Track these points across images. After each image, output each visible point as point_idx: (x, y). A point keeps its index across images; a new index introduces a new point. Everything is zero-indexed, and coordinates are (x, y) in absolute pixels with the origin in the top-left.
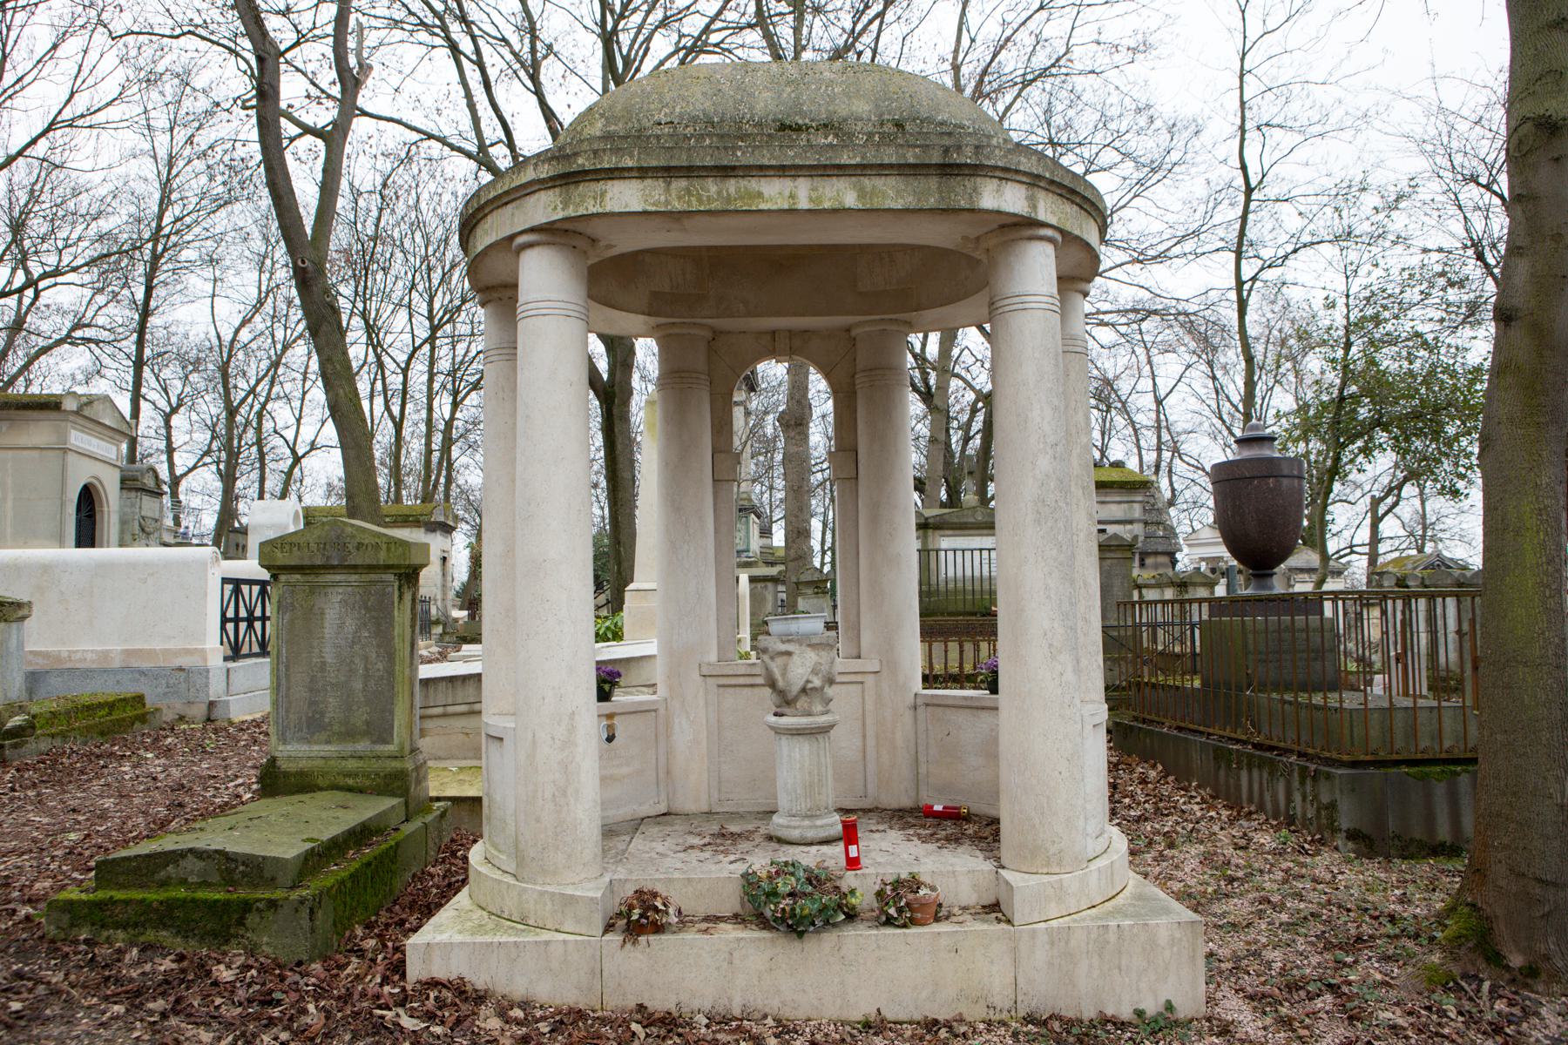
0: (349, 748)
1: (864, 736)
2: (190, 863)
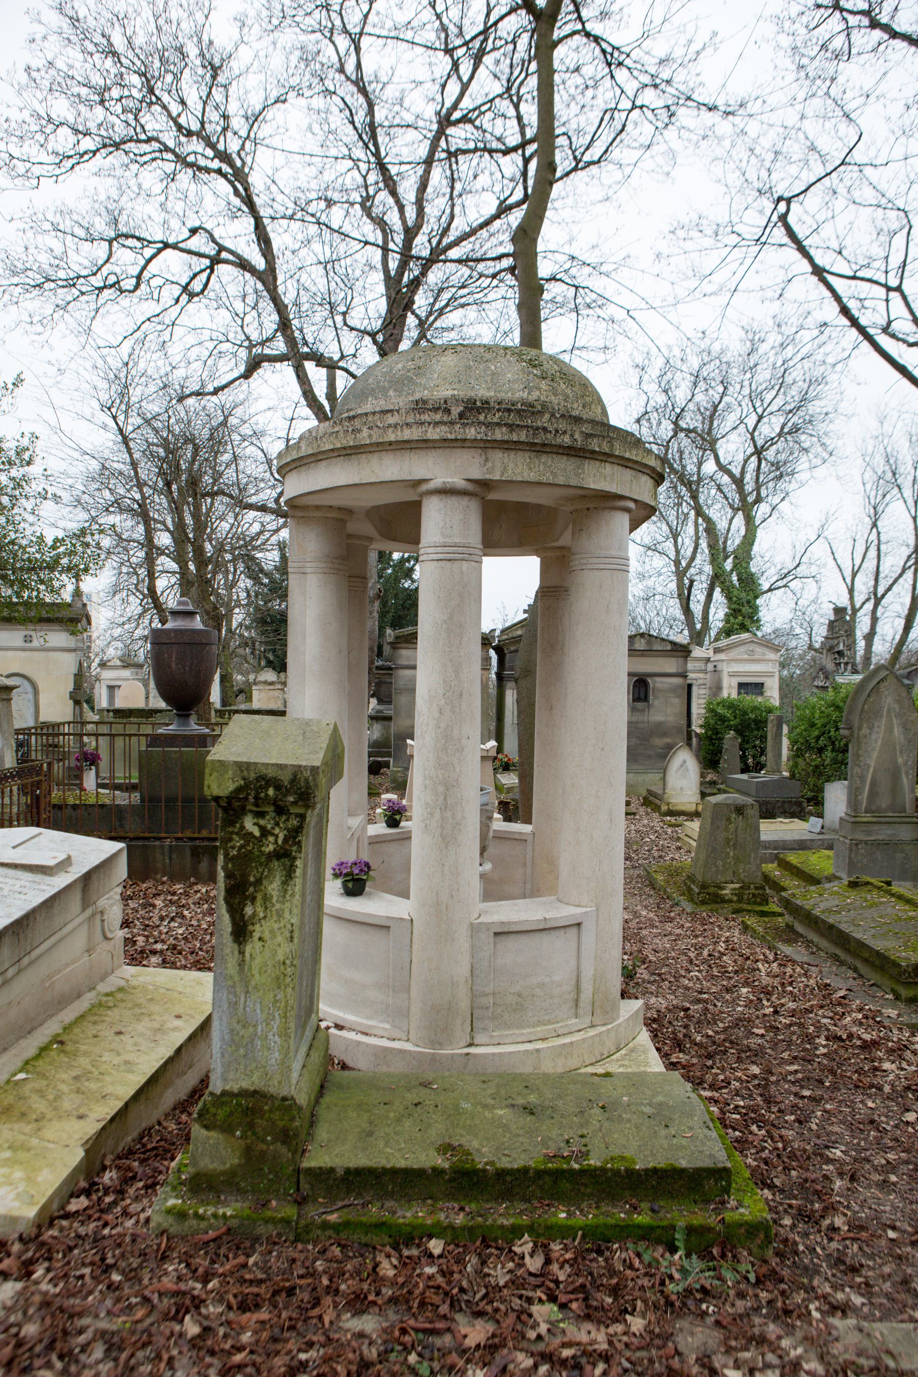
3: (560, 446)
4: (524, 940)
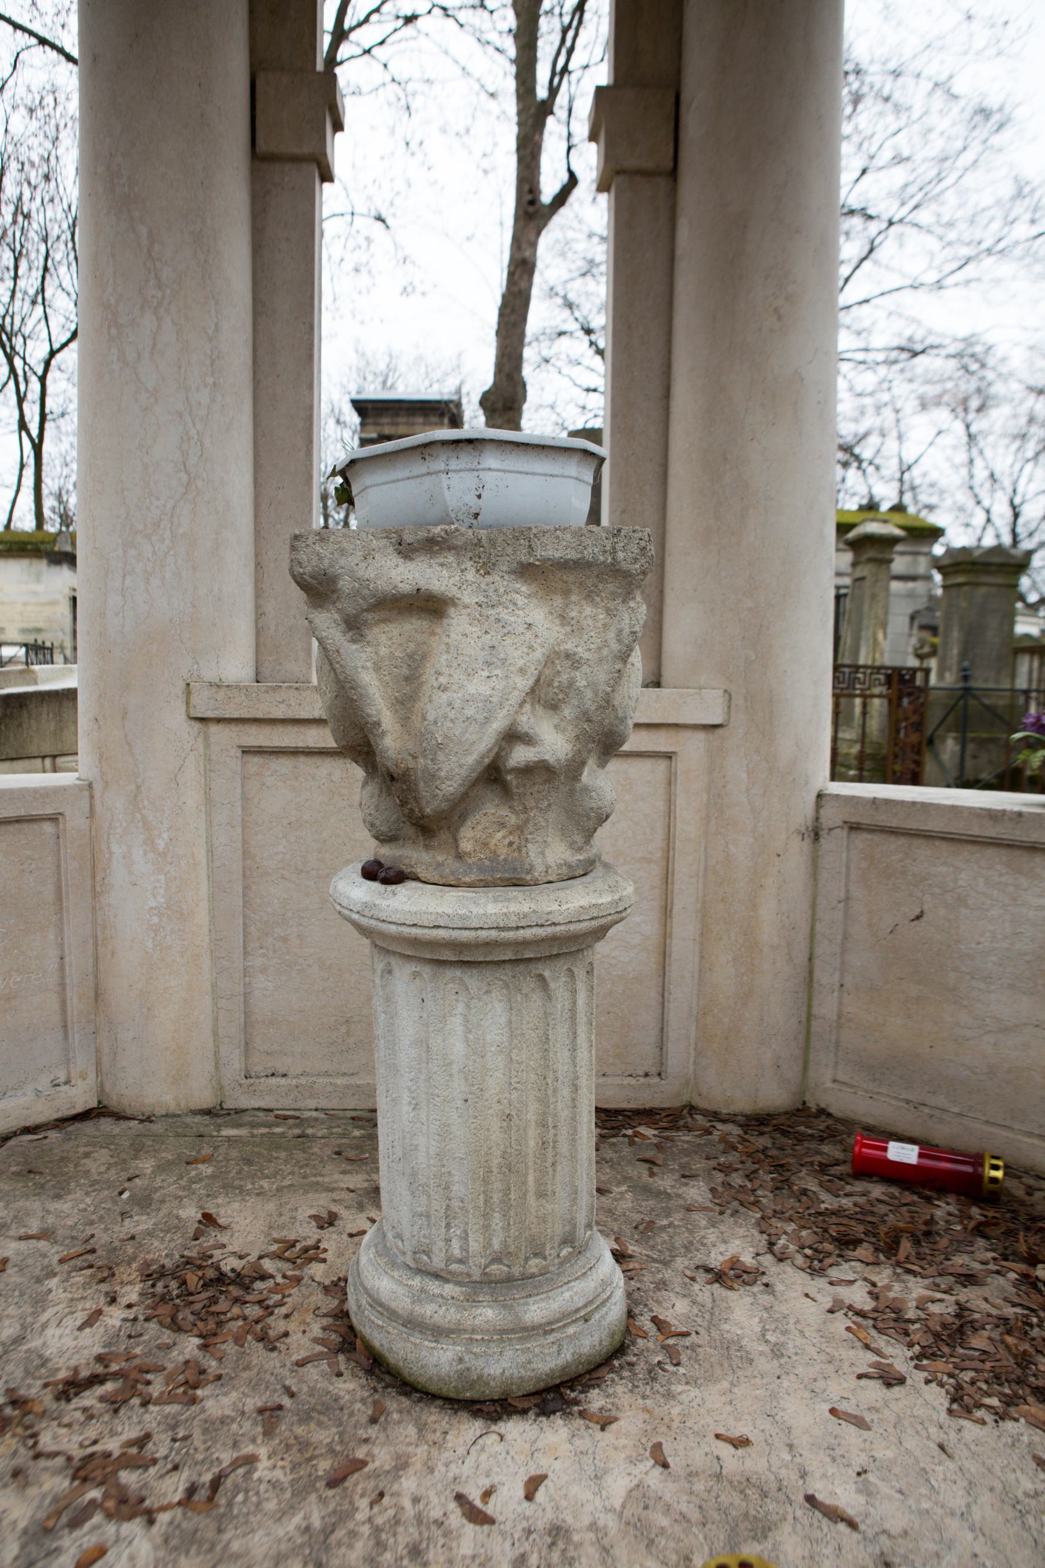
1: (666, 912)
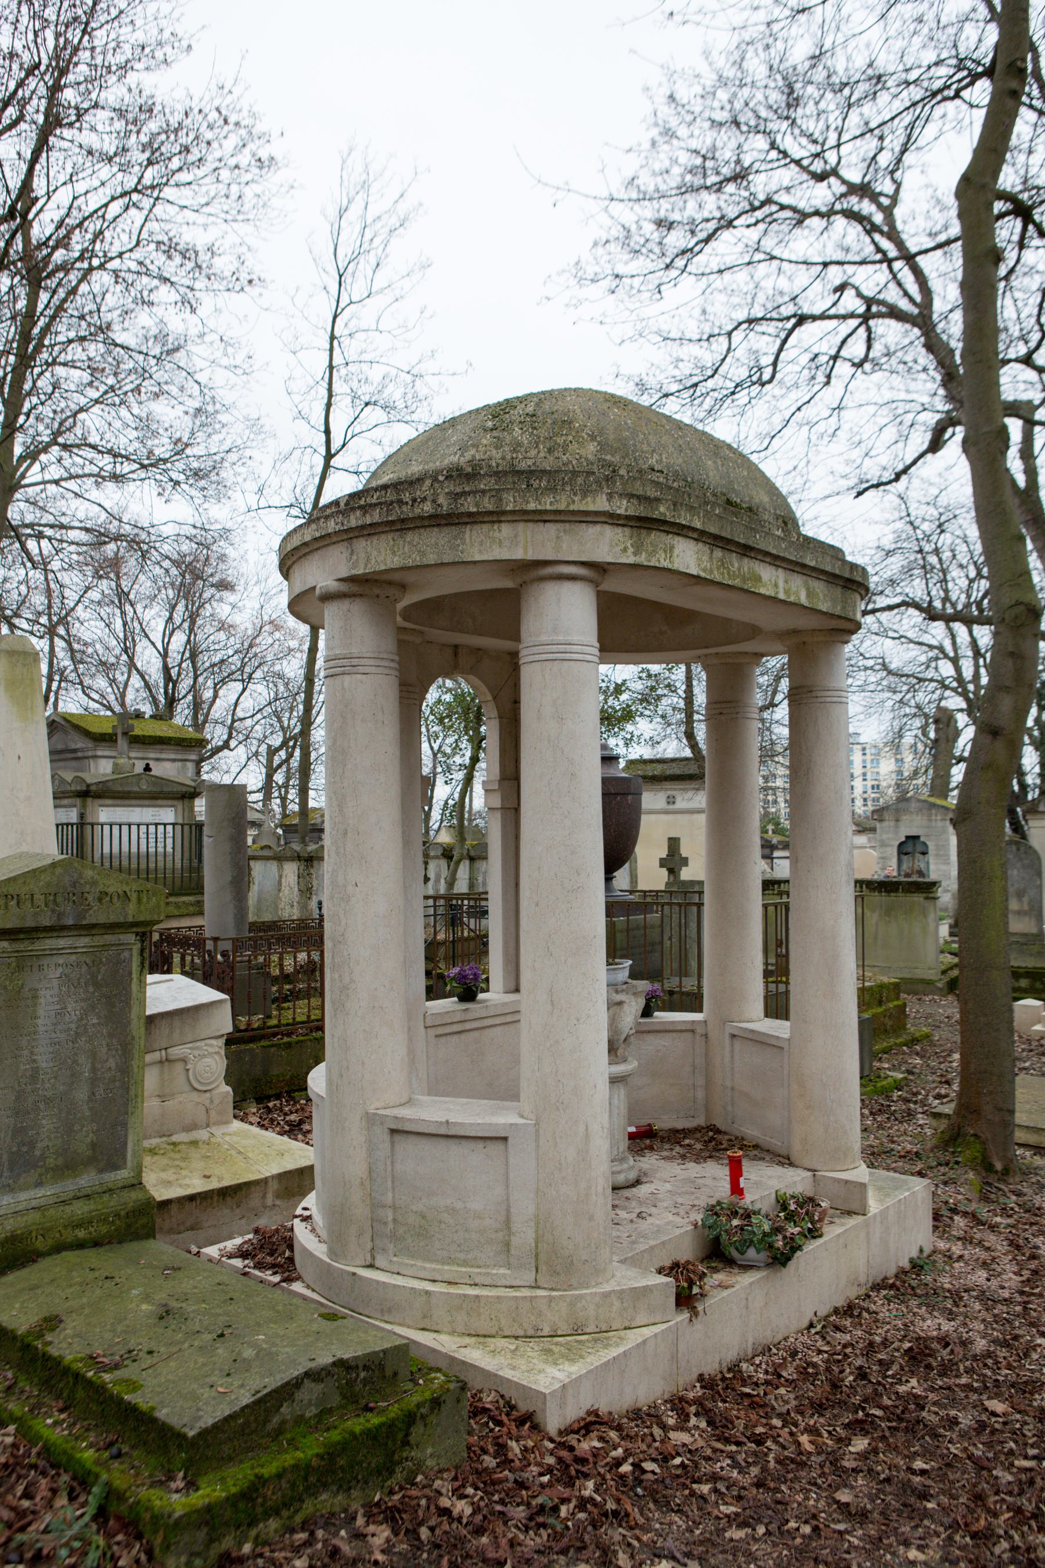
0: (69, 1186)
2: (310, 1392)
3: (421, 518)
4: (425, 1144)
